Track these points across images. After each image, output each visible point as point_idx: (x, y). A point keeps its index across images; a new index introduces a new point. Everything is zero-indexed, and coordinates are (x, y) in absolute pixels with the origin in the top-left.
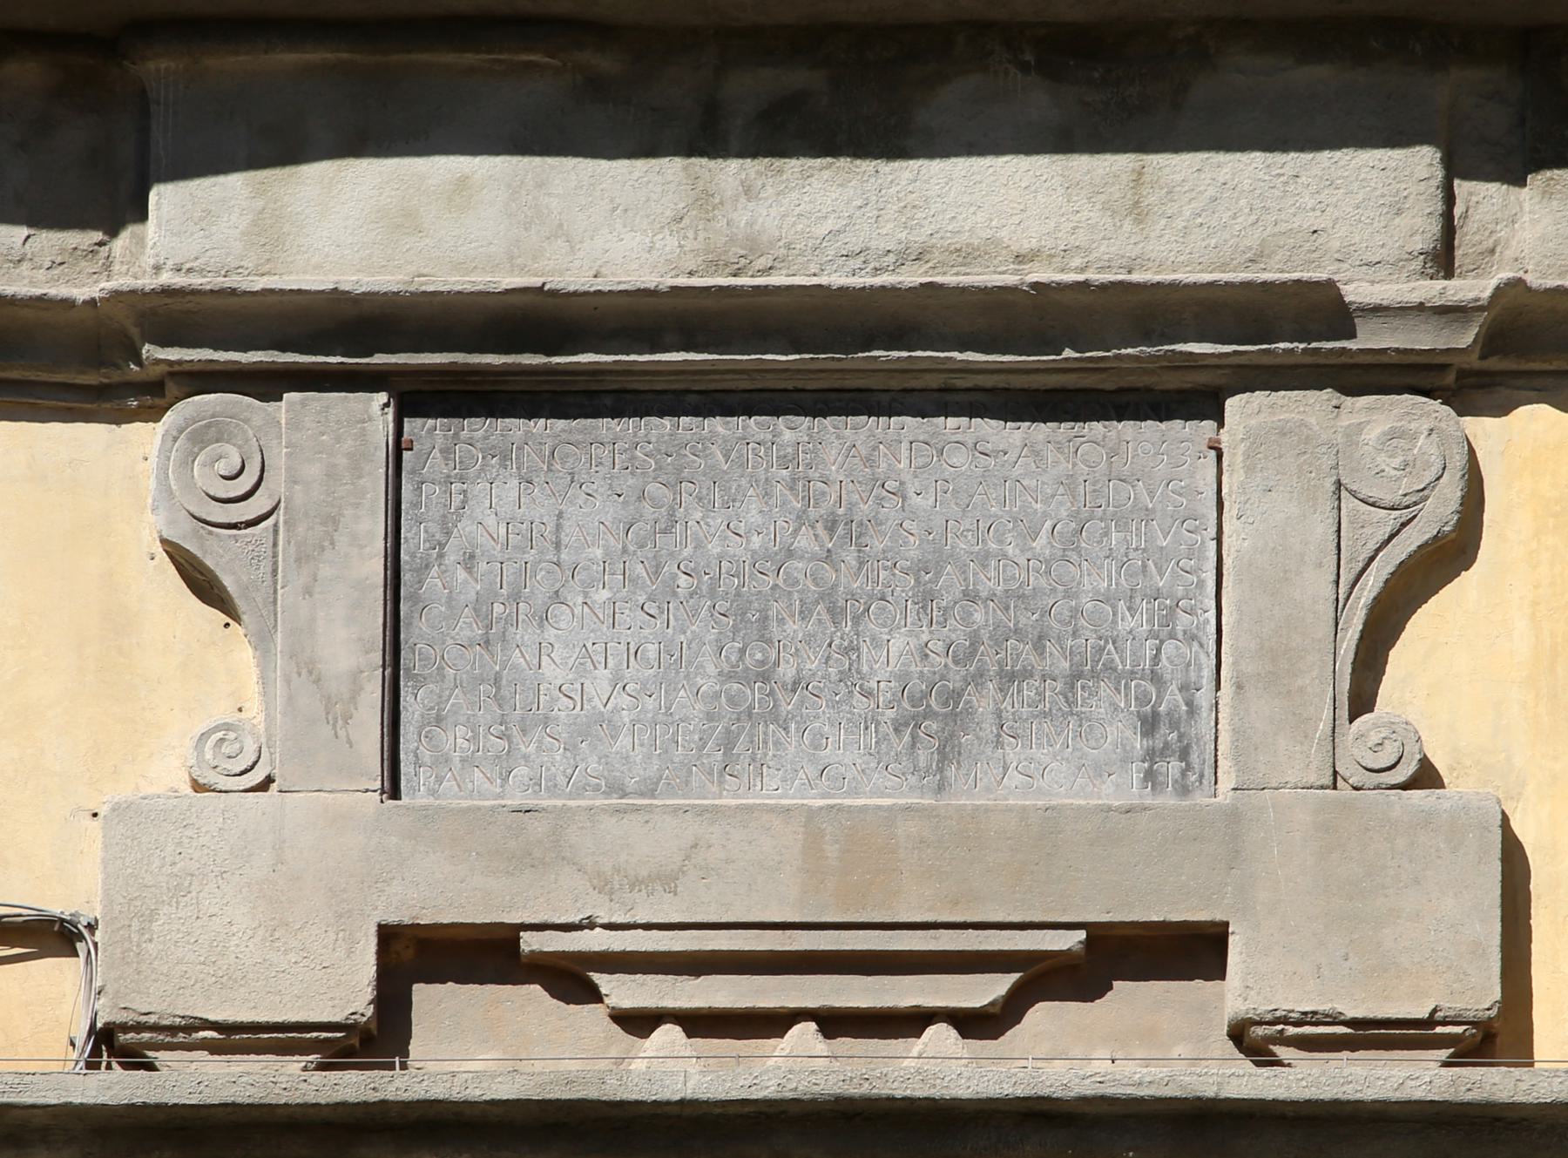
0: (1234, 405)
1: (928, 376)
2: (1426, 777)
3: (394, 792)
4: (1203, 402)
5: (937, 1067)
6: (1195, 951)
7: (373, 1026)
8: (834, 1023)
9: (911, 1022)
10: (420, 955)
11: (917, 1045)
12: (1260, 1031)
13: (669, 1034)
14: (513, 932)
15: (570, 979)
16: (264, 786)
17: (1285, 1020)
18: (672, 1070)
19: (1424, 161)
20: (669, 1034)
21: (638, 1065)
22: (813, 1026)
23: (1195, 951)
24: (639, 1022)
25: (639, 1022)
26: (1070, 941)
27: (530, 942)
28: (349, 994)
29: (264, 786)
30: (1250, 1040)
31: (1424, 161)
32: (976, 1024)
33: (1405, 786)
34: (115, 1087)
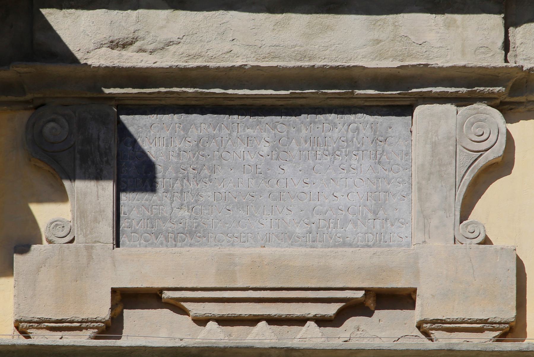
0: (420, 110)
1: (301, 100)
2: (486, 241)
3: (118, 245)
4: (405, 109)
5: (310, 336)
6: (401, 299)
7: (110, 322)
8: (273, 321)
9: (301, 321)
10: (127, 299)
11: (304, 328)
12: (25, 325)
13: (212, 325)
14: (161, 290)
15: (176, 306)
16: (72, 241)
17: (495, 323)
18: (214, 335)
19: (108, 188)
20: (212, 325)
21: (249, 337)
22: (264, 323)
23: (401, 299)
24: (201, 321)
25: (201, 321)
26: (360, 294)
27: (167, 295)
28: (102, 310)
29: (72, 241)
30: (425, 328)
31: (108, 188)
32: (322, 321)
33: (479, 244)
34: (22, 341)
